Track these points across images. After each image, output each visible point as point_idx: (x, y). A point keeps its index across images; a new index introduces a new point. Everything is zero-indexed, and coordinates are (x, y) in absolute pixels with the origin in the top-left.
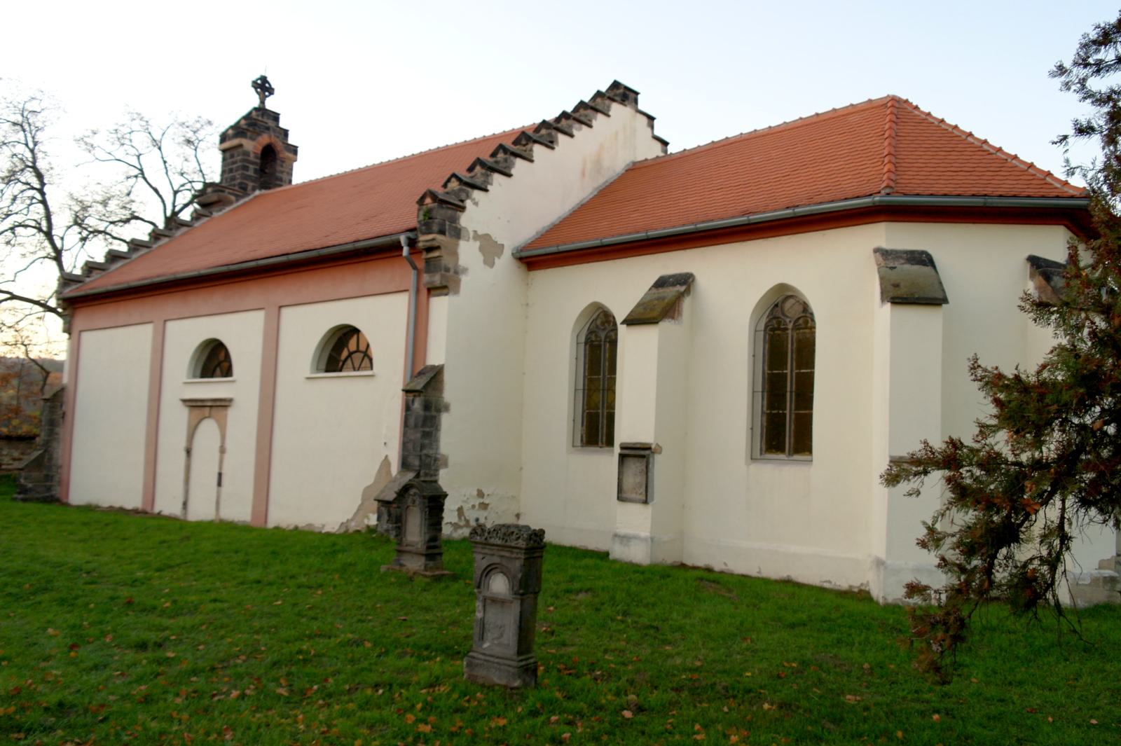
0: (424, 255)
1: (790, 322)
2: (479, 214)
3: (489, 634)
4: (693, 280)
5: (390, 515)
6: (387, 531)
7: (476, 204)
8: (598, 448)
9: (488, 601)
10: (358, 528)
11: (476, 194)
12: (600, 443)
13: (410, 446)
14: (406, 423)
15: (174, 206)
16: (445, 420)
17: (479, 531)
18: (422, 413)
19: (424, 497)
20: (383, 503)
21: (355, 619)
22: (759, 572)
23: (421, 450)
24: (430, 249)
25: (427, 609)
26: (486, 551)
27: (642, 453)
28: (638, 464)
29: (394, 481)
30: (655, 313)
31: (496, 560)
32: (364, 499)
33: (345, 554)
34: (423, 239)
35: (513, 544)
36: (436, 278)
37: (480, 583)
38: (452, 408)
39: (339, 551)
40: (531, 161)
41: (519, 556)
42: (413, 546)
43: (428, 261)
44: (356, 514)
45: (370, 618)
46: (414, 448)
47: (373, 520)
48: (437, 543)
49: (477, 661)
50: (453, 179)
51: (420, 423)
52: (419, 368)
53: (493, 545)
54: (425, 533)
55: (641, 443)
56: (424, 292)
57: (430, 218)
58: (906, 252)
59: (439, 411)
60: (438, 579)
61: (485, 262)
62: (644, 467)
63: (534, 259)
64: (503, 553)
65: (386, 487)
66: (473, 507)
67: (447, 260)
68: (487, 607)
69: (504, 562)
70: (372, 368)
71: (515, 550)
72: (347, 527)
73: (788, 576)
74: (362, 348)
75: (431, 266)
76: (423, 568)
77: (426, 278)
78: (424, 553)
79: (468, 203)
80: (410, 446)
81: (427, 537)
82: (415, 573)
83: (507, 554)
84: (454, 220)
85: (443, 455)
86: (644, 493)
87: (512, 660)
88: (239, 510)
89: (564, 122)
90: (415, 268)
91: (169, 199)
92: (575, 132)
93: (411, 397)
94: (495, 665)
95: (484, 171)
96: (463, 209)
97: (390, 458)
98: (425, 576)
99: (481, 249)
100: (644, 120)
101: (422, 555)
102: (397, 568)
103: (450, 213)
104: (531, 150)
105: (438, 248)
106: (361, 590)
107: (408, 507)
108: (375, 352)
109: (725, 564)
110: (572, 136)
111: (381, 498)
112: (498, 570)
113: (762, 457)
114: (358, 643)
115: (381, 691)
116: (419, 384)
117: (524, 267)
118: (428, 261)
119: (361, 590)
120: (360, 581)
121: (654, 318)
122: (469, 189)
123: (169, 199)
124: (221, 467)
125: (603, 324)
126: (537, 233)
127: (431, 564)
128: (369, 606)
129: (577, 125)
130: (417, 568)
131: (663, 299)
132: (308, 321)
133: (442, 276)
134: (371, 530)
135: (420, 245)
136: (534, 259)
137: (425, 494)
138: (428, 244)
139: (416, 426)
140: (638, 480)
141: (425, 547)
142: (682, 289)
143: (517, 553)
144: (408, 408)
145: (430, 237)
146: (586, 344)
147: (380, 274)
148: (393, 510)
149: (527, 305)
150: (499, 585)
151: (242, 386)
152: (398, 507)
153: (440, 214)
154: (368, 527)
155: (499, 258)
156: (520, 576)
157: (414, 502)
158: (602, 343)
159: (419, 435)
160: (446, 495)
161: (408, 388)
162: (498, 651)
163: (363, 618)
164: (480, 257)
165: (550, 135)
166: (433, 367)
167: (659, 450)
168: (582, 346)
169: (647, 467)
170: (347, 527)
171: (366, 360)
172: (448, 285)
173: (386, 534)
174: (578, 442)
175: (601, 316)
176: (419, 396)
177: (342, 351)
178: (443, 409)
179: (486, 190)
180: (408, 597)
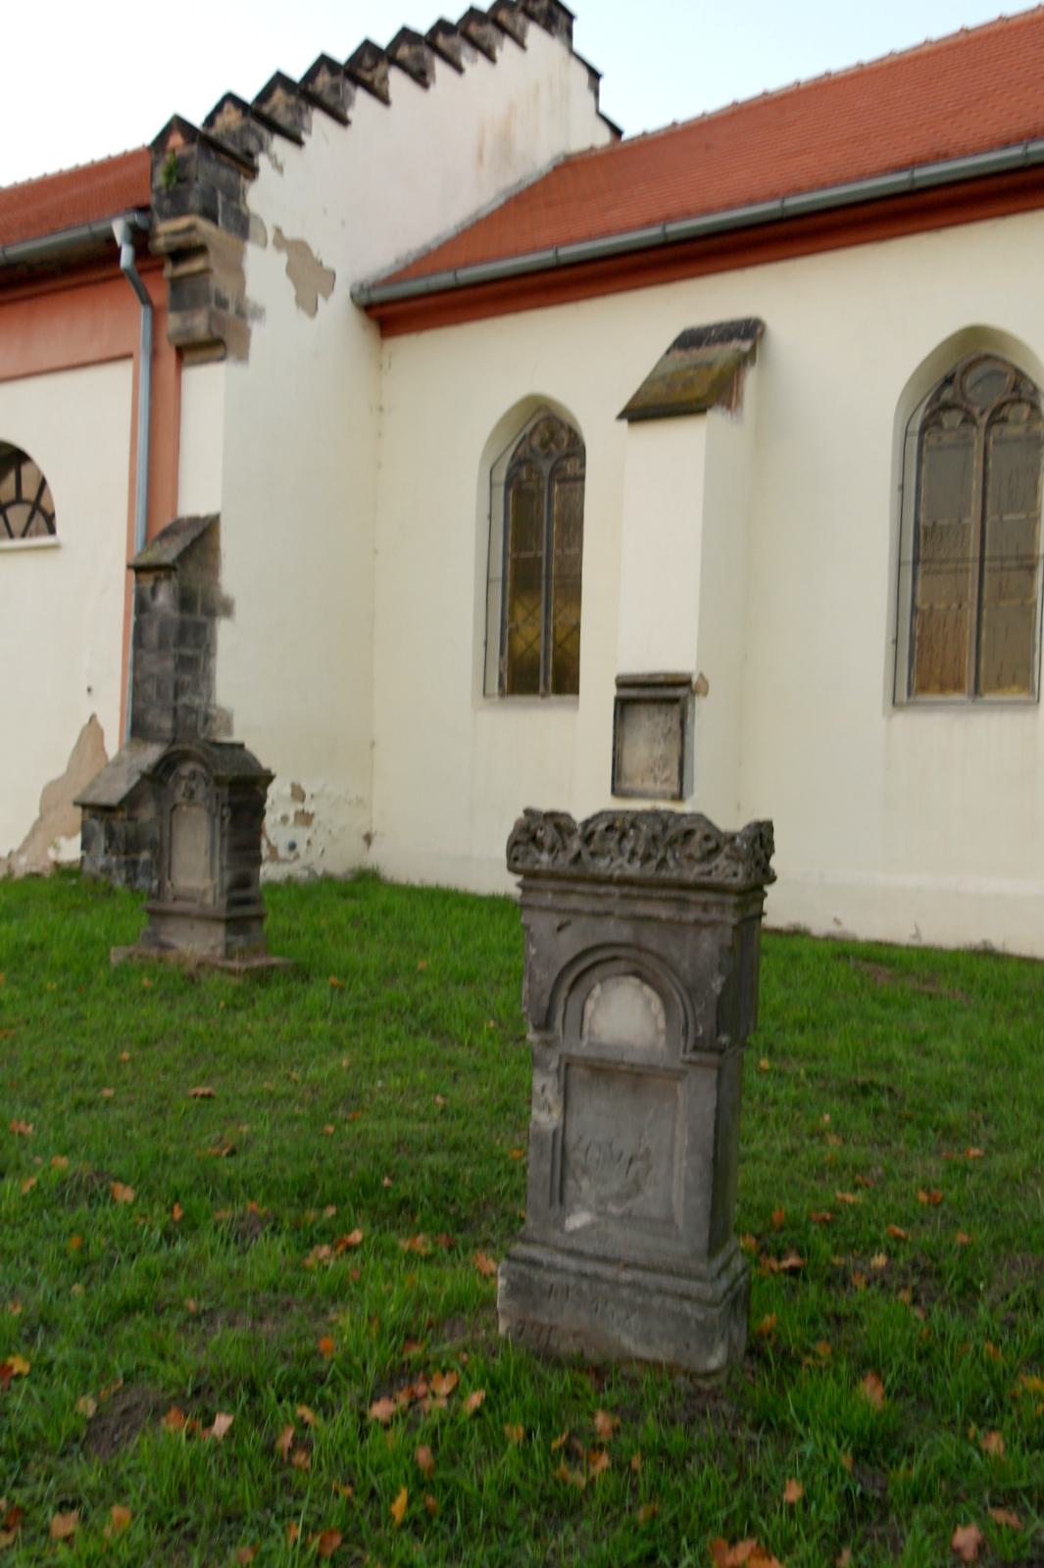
0: (169, 271)
1: (982, 413)
2: (285, 187)
3: (585, 1183)
4: (762, 333)
5: (111, 835)
6: (107, 870)
7: (279, 168)
8: (538, 699)
9: (579, 1073)
10: (35, 869)
11: (279, 145)
12: (542, 688)
13: (150, 688)
14: (139, 639)
16: (225, 633)
17: (547, 834)
18: (175, 615)
19: (218, 781)
20: (96, 811)
21: (67, 1100)
22: (917, 935)
23: (176, 697)
24: (180, 254)
25: (261, 1061)
26: (574, 902)
27: (670, 693)
28: (660, 719)
29: (118, 762)
30: (699, 391)
31: (616, 931)
32: (46, 808)
33: (15, 923)
34: (167, 230)
35: (692, 874)
36: (202, 328)
37: (550, 1012)
38: (239, 608)
41: (714, 914)
42: (192, 899)
43: (176, 283)
44: (28, 841)
45: (108, 1093)
46: (159, 694)
47: (70, 850)
48: (250, 893)
49: (552, 1279)
50: (228, 106)
51: (172, 639)
52: (164, 521)
53: (609, 881)
54: (222, 869)
55: (666, 675)
56: (169, 357)
57: (180, 180)
59: (211, 613)
60: (262, 977)
61: (300, 302)
62: (676, 726)
63: (397, 310)
64: (642, 908)
65: (99, 776)
66: (285, 819)
67: (219, 281)
68: (576, 1101)
69: (652, 939)
70: (52, 531)
71: (693, 896)
72: (9, 867)
73: (985, 942)
74: (29, 491)
75: (185, 294)
76: (220, 951)
77: (173, 322)
78: (224, 915)
79: (262, 161)
80: (150, 688)
81: (228, 878)
82: (200, 965)
83: (663, 912)
84: (235, 195)
85: (222, 711)
86: (675, 778)
87: (690, 1276)
90: (146, 300)
93: (148, 581)
94: (625, 1293)
95: (292, 100)
96: (252, 172)
97: (101, 720)
98: (232, 972)
99: (291, 270)
100: (584, 76)
101: (216, 920)
102: (154, 952)
104: (385, 78)
105: (200, 250)
106: (67, 1012)
107: (175, 806)
108: (60, 499)
109: (837, 921)
111: (90, 799)
112: (622, 966)
113: (912, 699)
114: (92, 1190)
115: (222, 1423)
116: (168, 552)
117: (373, 331)
118: (176, 283)
119: (67, 1012)
120: (62, 989)
121: (698, 401)
122: (265, 133)
125: (544, 445)
126: (397, 261)
127: (240, 941)
128: (102, 1059)
130: (206, 952)
131: (710, 366)
133: (212, 316)
134: (63, 871)
135: (160, 243)
136: (397, 310)
137: (221, 773)
138: (180, 240)
139: (162, 644)
140: (659, 750)
141: (224, 901)
142: (746, 346)
143: (705, 907)
144: (142, 605)
145: (183, 222)
146: (508, 485)
147: (64, 325)
148: (118, 826)
149: (381, 409)
150: (624, 1016)
152: (131, 819)
153: (206, 171)
154: (57, 865)
155: (326, 297)
156: (717, 984)
157: (191, 794)
158: (545, 484)
159: (170, 664)
160: (269, 778)
161: (143, 561)
162: (623, 1240)
163: (89, 1094)
164: (288, 291)
165: (418, 57)
166: (194, 521)
167: (703, 688)
168: (500, 491)
169: (682, 724)
170: (9, 867)
171: (39, 520)
172: (226, 338)
173: (103, 878)
174: (494, 687)
175: (541, 427)
176: (169, 578)
178: (219, 610)
179: (298, 141)
180: (197, 1026)
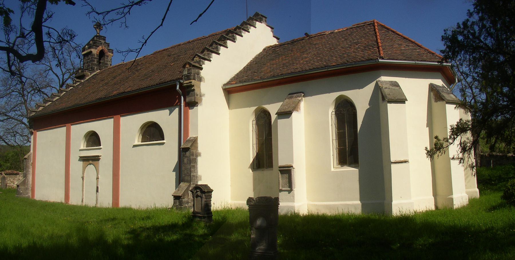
15: (63, 80)
39: (472, 91)
40: (227, 47)
58: (390, 82)
84: (198, 74)
88: (105, 201)
89: (238, 30)
91: (61, 77)
92: (243, 34)
103: (197, 70)
110: (242, 36)
123: (61, 77)
124: (97, 184)
129: (244, 32)
132: (132, 123)
151: (105, 151)
177: (152, 133)
